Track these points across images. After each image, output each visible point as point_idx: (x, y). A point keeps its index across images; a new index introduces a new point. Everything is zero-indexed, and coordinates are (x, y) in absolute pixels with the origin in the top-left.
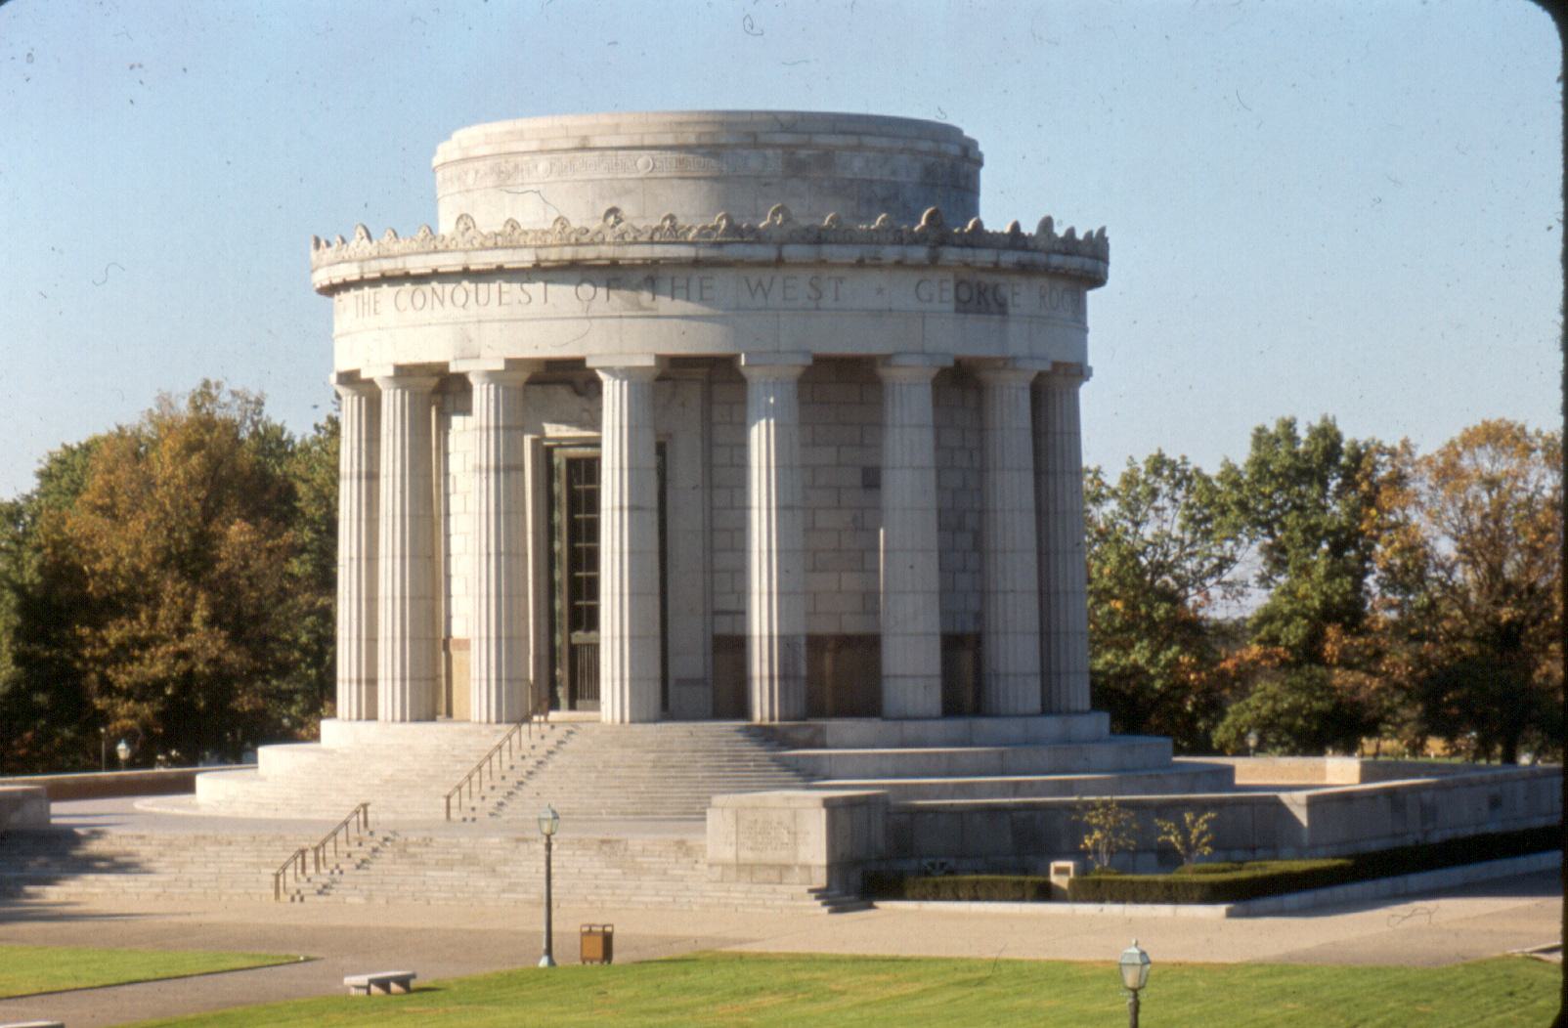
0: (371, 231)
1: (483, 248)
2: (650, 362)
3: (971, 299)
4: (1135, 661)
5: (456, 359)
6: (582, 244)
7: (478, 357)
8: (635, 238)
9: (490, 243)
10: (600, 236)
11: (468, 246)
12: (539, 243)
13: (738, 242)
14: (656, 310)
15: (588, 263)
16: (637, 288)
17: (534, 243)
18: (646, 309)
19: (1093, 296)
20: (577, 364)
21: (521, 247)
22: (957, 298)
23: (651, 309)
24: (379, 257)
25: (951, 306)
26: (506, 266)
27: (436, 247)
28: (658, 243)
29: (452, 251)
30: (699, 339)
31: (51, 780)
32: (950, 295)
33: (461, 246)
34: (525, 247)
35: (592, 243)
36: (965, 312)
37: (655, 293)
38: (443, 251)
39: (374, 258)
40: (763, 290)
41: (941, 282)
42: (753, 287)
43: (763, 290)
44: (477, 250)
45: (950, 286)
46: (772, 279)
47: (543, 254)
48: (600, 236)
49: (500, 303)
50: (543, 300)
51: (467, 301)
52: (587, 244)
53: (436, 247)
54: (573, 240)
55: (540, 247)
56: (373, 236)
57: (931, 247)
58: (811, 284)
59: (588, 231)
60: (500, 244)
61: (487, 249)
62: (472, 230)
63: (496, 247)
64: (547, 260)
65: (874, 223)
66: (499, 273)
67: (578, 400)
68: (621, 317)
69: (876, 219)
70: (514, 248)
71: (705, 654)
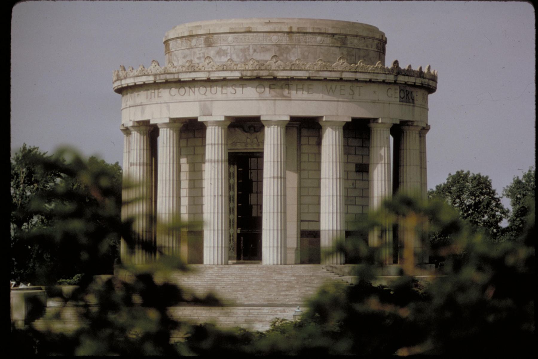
0: (159, 63)
1: (218, 70)
2: (288, 119)
3: (404, 96)
4: (50, 205)
5: (200, 116)
6: (261, 70)
7: (211, 115)
8: (284, 68)
9: (221, 69)
10: (270, 66)
11: (210, 69)
12: (242, 69)
13: (384, 73)
14: (290, 97)
15: (263, 77)
16: (282, 88)
17: (240, 69)
18: (285, 97)
19: (430, 96)
20: (257, 119)
21: (235, 70)
22: (400, 97)
23: (288, 97)
24: (165, 73)
25: (398, 100)
26: (227, 78)
27: (194, 70)
28: (294, 70)
29: (202, 71)
30: (362, 113)
31: (29, 293)
32: (398, 95)
33: (206, 69)
34: (237, 70)
35: (266, 69)
36: (403, 102)
37: (289, 89)
38: (198, 71)
39: (162, 74)
40: (332, 91)
41: (395, 89)
42: (329, 90)
43: (332, 91)
44: (215, 71)
45: (398, 91)
46: (336, 86)
47: (244, 73)
48: (270, 66)
49: (222, 93)
50: (242, 93)
51: (206, 92)
52: (264, 70)
53: (194, 70)
54: (258, 68)
55: (243, 71)
56: (160, 64)
57: (395, 75)
58: (351, 89)
59: (264, 65)
60: (225, 69)
61: (219, 71)
62: (212, 63)
63: (223, 70)
64: (246, 76)
65: (375, 65)
66: (224, 82)
67: (246, 134)
68: (338, 101)
69: (376, 63)
70: (232, 71)
71: (297, 238)
